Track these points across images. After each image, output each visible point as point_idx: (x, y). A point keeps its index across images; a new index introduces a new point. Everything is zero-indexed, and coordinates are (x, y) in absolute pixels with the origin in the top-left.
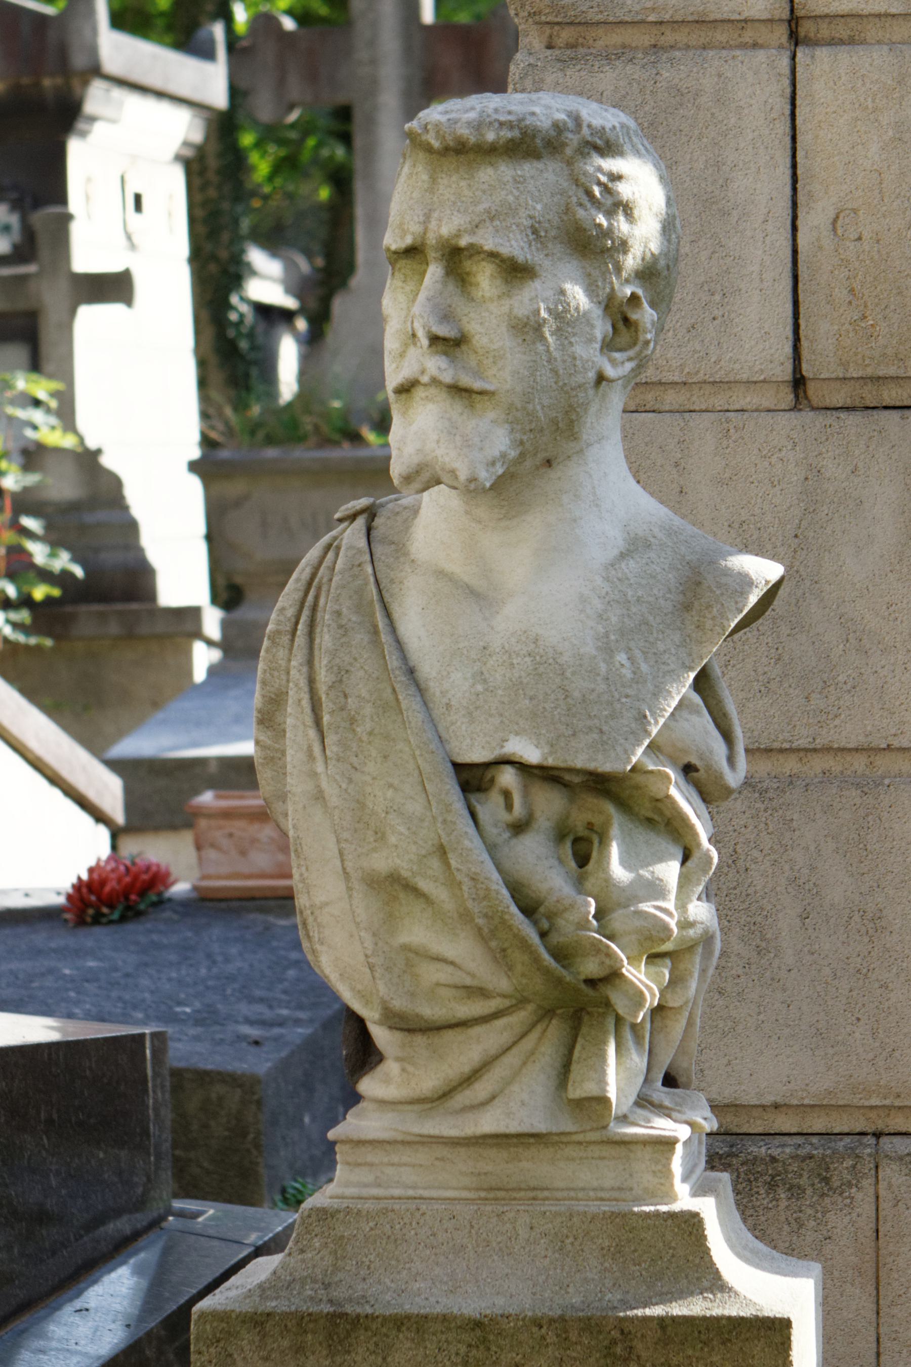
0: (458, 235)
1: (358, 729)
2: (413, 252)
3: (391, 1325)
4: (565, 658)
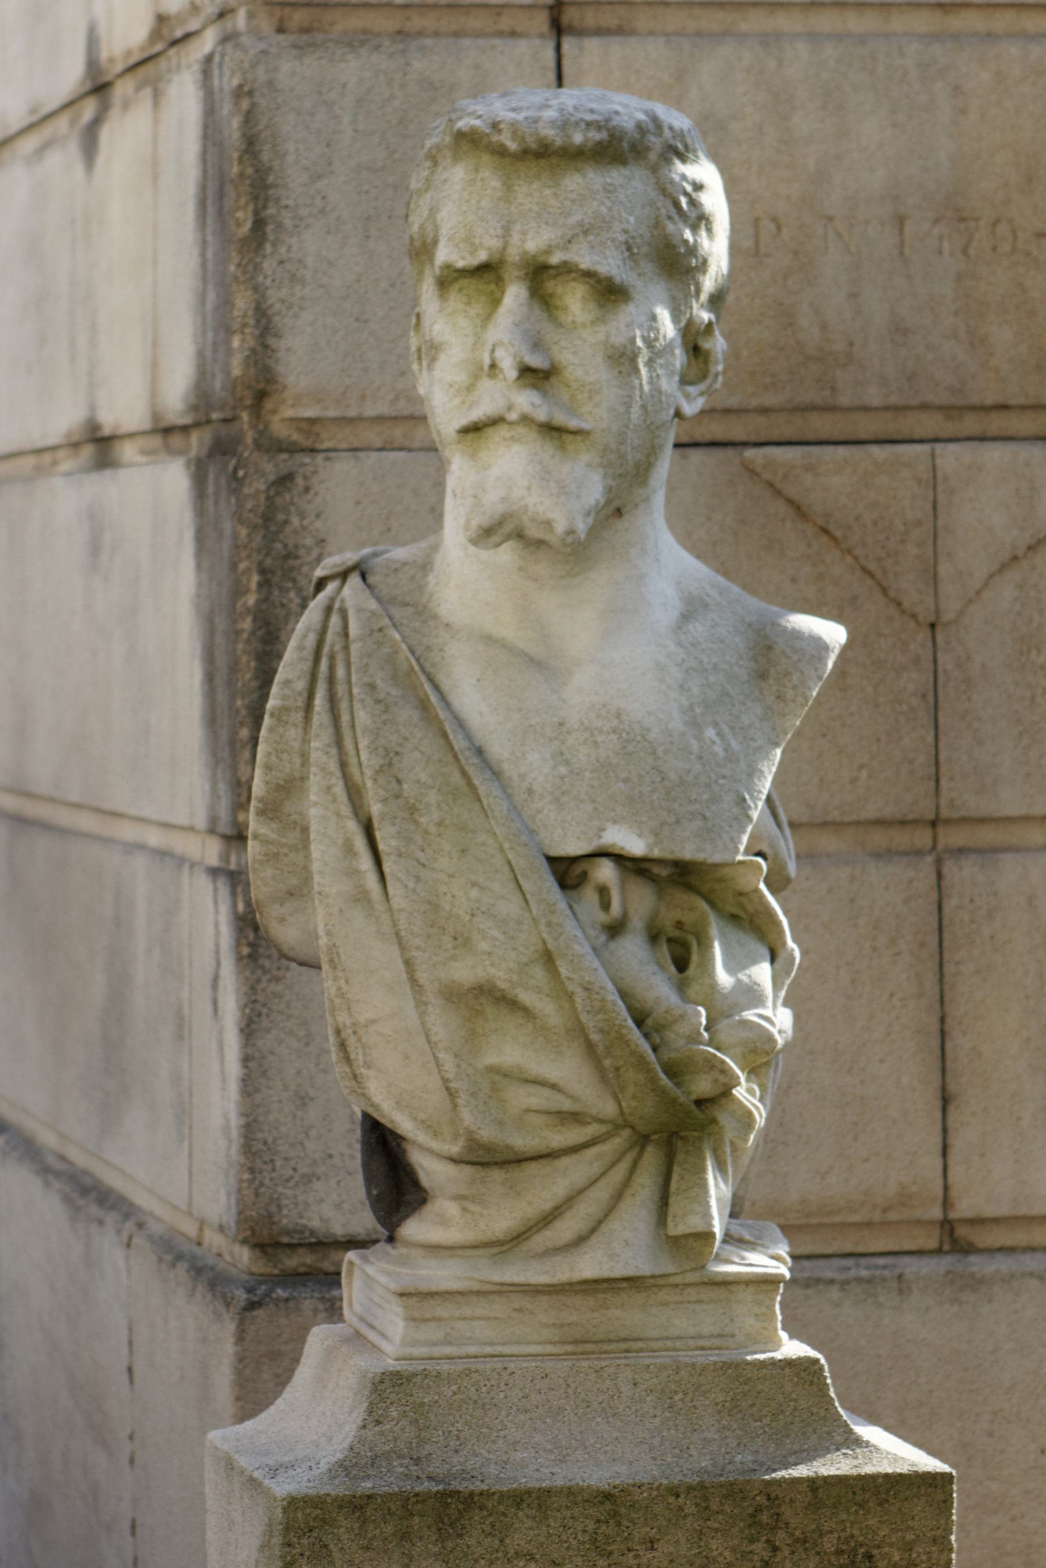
0: (548, 252)
1: (423, 820)
2: (488, 271)
3: (510, 1502)
4: (654, 735)
